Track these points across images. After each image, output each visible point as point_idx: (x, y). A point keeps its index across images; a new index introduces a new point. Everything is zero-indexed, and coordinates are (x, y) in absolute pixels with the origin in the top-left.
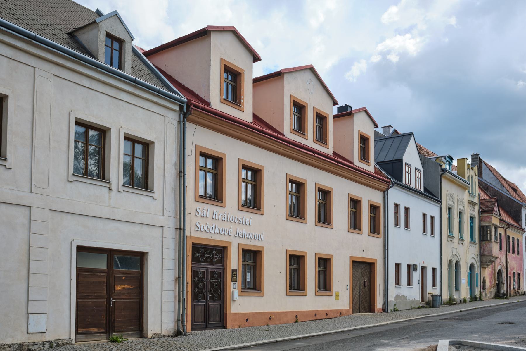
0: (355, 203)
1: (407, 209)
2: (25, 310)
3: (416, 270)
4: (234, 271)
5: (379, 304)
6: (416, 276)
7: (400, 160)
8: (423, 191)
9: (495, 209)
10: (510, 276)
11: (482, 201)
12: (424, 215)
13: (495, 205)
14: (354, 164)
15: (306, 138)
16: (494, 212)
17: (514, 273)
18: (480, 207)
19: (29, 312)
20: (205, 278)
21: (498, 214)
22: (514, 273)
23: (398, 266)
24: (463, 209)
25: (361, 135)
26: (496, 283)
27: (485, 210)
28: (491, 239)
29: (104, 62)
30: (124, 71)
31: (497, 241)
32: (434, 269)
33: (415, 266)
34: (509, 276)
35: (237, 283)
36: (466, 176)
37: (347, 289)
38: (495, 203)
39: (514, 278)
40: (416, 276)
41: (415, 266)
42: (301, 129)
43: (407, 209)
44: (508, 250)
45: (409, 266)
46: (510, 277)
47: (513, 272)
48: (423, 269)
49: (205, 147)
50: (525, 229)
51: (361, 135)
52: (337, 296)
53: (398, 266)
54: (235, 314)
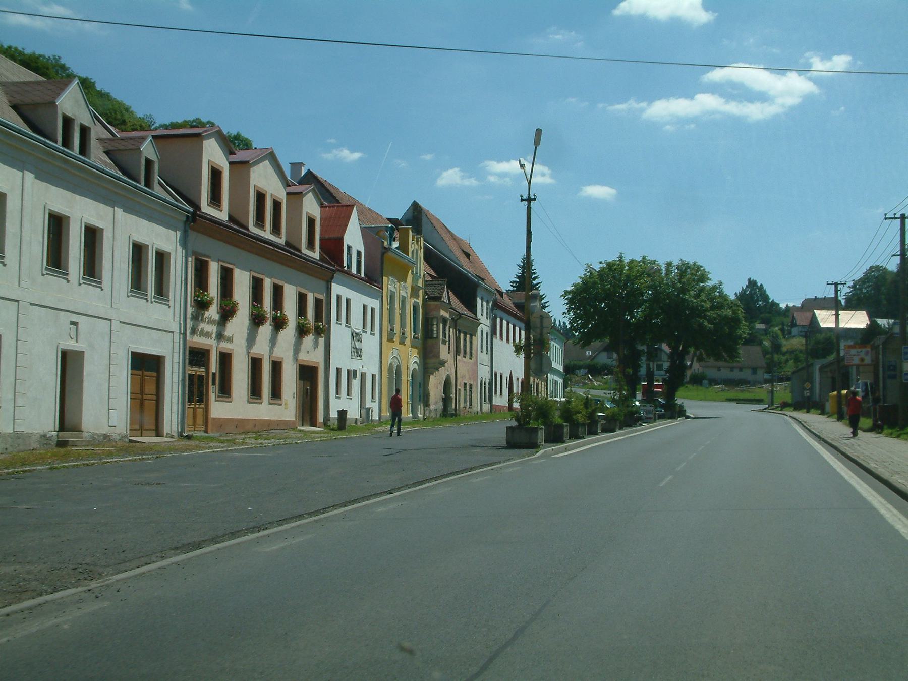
0: (138, 250)
1: (348, 301)
2: (107, 408)
3: (355, 376)
4: (214, 374)
5: (321, 418)
6: (356, 383)
7: (340, 241)
8: (356, 273)
9: (444, 296)
10: (460, 388)
11: (428, 283)
12: (365, 307)
13: (444, 290)
14: (303, 252)
15: (265, 229)
16: (443, 300)
17: (465, 384)
18: (426, 293)
19: (110, 408)
20: (812, 383)
21: (448, 302)
22: (465, 384)
23: (338, 371)
24: (405, 296)
25: (309, 217)
26: (443, 398)
27: (431, 295)
28: (438, 337)
29: (78, 153)
30: (153, 190)
31: (446, 338)
32: (373, 376)
33: (355, 371)
34: (458, 387)
35: (215, 386)
36: (411, 250)
37: (294, 398)
38: (444, 288)
39: (465, 392)
40: (356, 383)
41: (355, 371)
42: (260, 220)
43: (348, 301)
44: (457, 352)
45: (348, 371)
46: (459, 389)
47: (464, 383)
48: (363, 375)
49: (887, 488)
50: (132, 107)
51: (309, 217)
52: (286, 404)
53: (338, 371)
54: (214, 419)
